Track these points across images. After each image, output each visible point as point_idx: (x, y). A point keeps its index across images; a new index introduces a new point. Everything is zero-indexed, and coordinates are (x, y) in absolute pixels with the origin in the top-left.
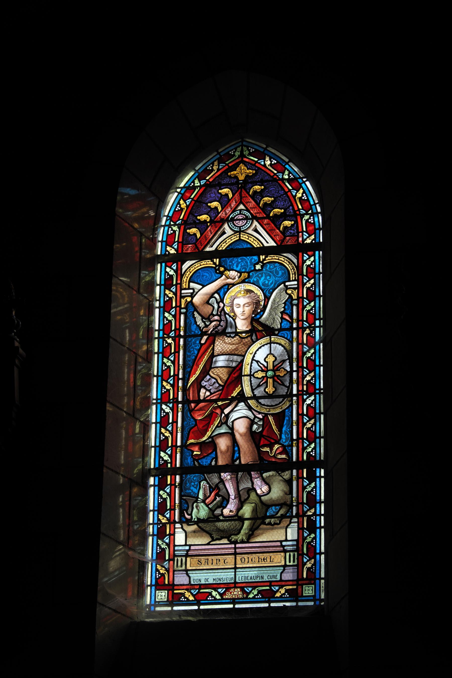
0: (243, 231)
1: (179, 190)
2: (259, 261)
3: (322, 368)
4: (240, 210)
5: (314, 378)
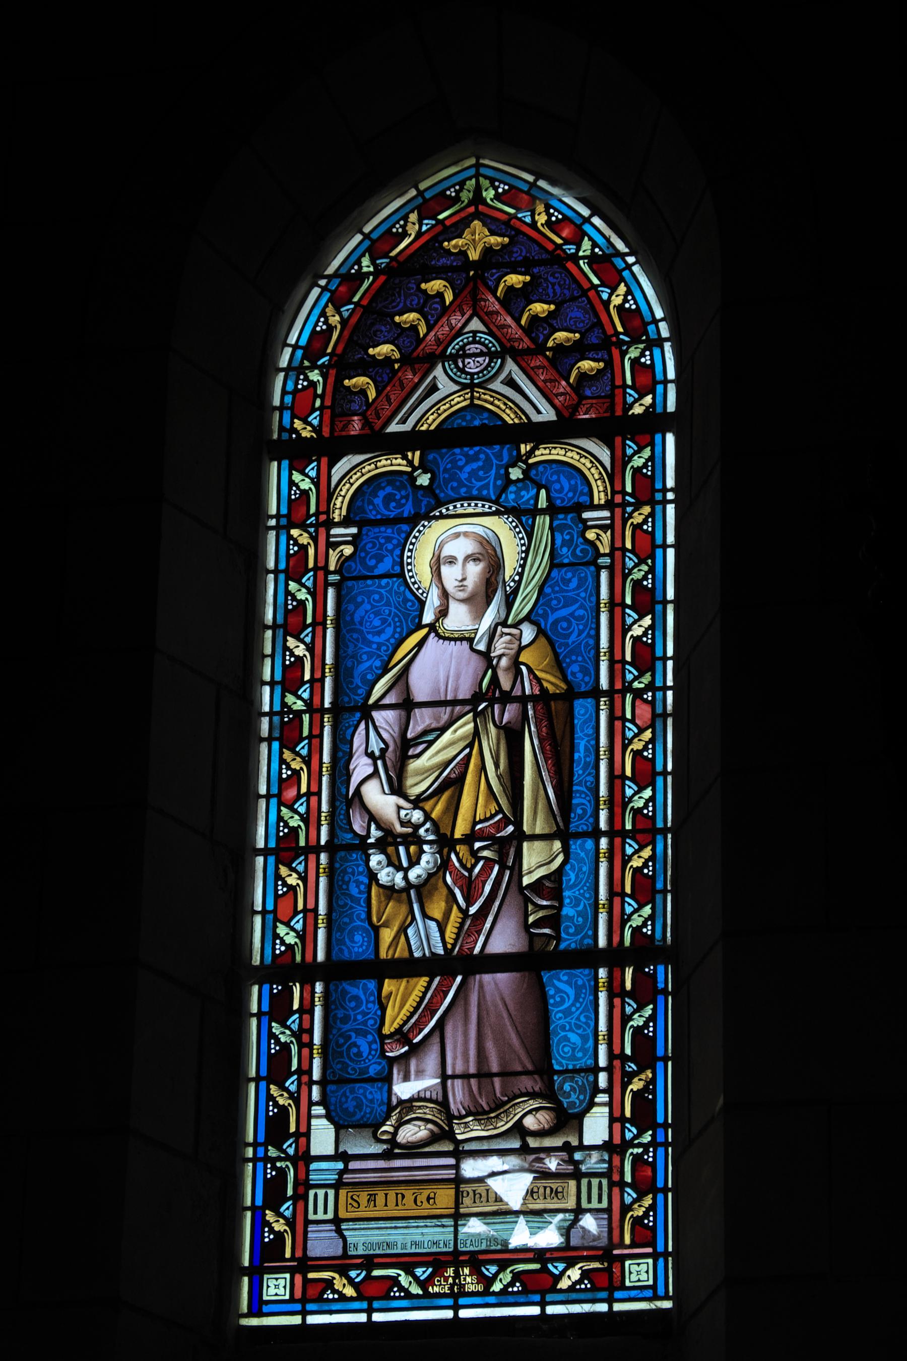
0: (480, 385)
1: (323, 282)
2: (519, 458)
3: (669, 779)
4: (475, 333)
5: (649, 923)
